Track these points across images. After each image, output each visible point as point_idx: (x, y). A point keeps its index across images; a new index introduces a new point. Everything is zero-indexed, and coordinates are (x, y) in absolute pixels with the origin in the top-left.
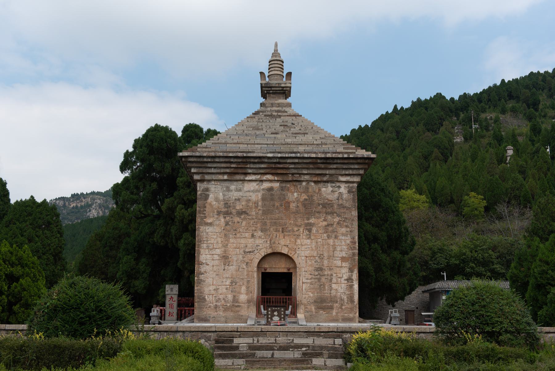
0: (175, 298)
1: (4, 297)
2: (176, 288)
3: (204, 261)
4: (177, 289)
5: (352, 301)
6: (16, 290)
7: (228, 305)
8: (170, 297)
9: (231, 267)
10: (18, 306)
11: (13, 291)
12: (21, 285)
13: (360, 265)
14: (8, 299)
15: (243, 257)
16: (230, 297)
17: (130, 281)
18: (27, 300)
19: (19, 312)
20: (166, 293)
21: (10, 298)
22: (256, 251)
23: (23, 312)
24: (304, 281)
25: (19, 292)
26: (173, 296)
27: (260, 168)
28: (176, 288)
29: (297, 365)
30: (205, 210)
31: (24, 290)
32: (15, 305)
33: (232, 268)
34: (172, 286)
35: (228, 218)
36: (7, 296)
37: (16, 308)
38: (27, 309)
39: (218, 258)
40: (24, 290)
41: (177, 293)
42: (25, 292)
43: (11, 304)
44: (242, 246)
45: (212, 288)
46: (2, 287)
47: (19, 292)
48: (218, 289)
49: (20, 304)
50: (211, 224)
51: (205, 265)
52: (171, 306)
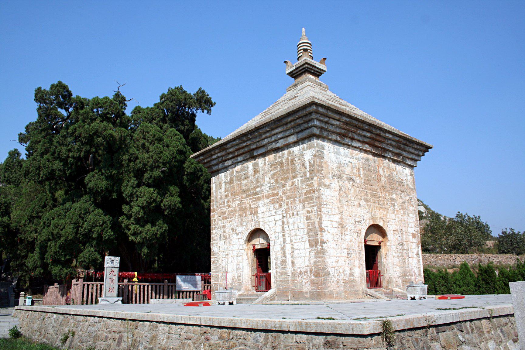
0: (116, 271)
2: (117, 260)
3: (326, 228)
4: (119, 262)
5: (421, 275)
7: (347, 279)
8: (109, 270)
9: (346, 237)
15: (355, 227)
16: (348, 271)
22: (363, 222)
24: (395, 254)
27: (365, 136)
28: (117, 260)
30: (322, 170)
33: (348, 238)
35: (341, 183)
39: (337, 226)
41: (119, 266)
44: (354, 214)
45: (334, 259)
48: (338, 261)
50: (328, 186)
51: (326, 233)
52: (111, 280)
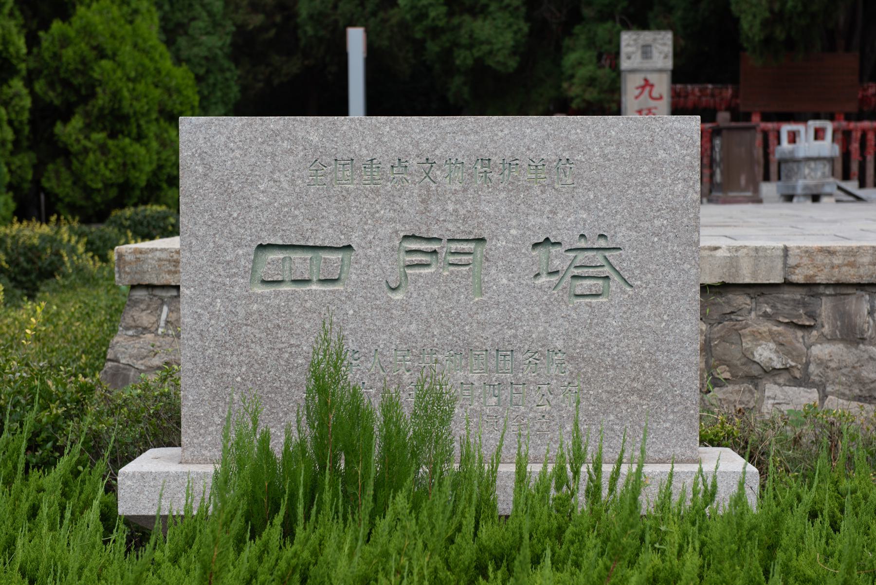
1: (17, 84)
4: (669, 49)
6: (68, 53)
10: (77, 121)
11: (56, 56)
12: (87, 31)
13: (197, 111)
14: (32, 93)
17: (456, 21)
18: (116, 95)
19: (86, 151)
20: (625, 64)
21: (39, 86)
23: (103, 149)
25: (83, 61)
26: (653, 78)
29: (305, 486)
31: (101, 54)
32: (66, 120)
34: (647, 36)
36: (29, 82)
37: (70, 131)
38: (113, 135)
40: (101, 54)
41: (669, 64)
42: (106, 64)
43: (45, 116)
46: (6, 42)
47: (83, 61)
49: (87, 115)
